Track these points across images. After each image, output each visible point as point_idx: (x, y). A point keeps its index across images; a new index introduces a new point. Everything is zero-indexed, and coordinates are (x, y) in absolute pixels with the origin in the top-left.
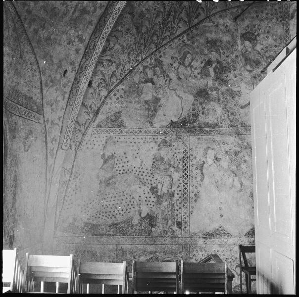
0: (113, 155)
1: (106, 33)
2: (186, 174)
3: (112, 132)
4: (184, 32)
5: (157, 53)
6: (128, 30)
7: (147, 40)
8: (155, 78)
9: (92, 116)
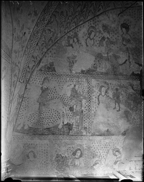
0: (47, 88)
1: (51, 11)
2: (89, 100)
3: (48, 74)
4: (91, 19)
5: (76, 29)
6: (62, 12)
7: (72, 20)
8: (74, 44)
9: (37, 64)
